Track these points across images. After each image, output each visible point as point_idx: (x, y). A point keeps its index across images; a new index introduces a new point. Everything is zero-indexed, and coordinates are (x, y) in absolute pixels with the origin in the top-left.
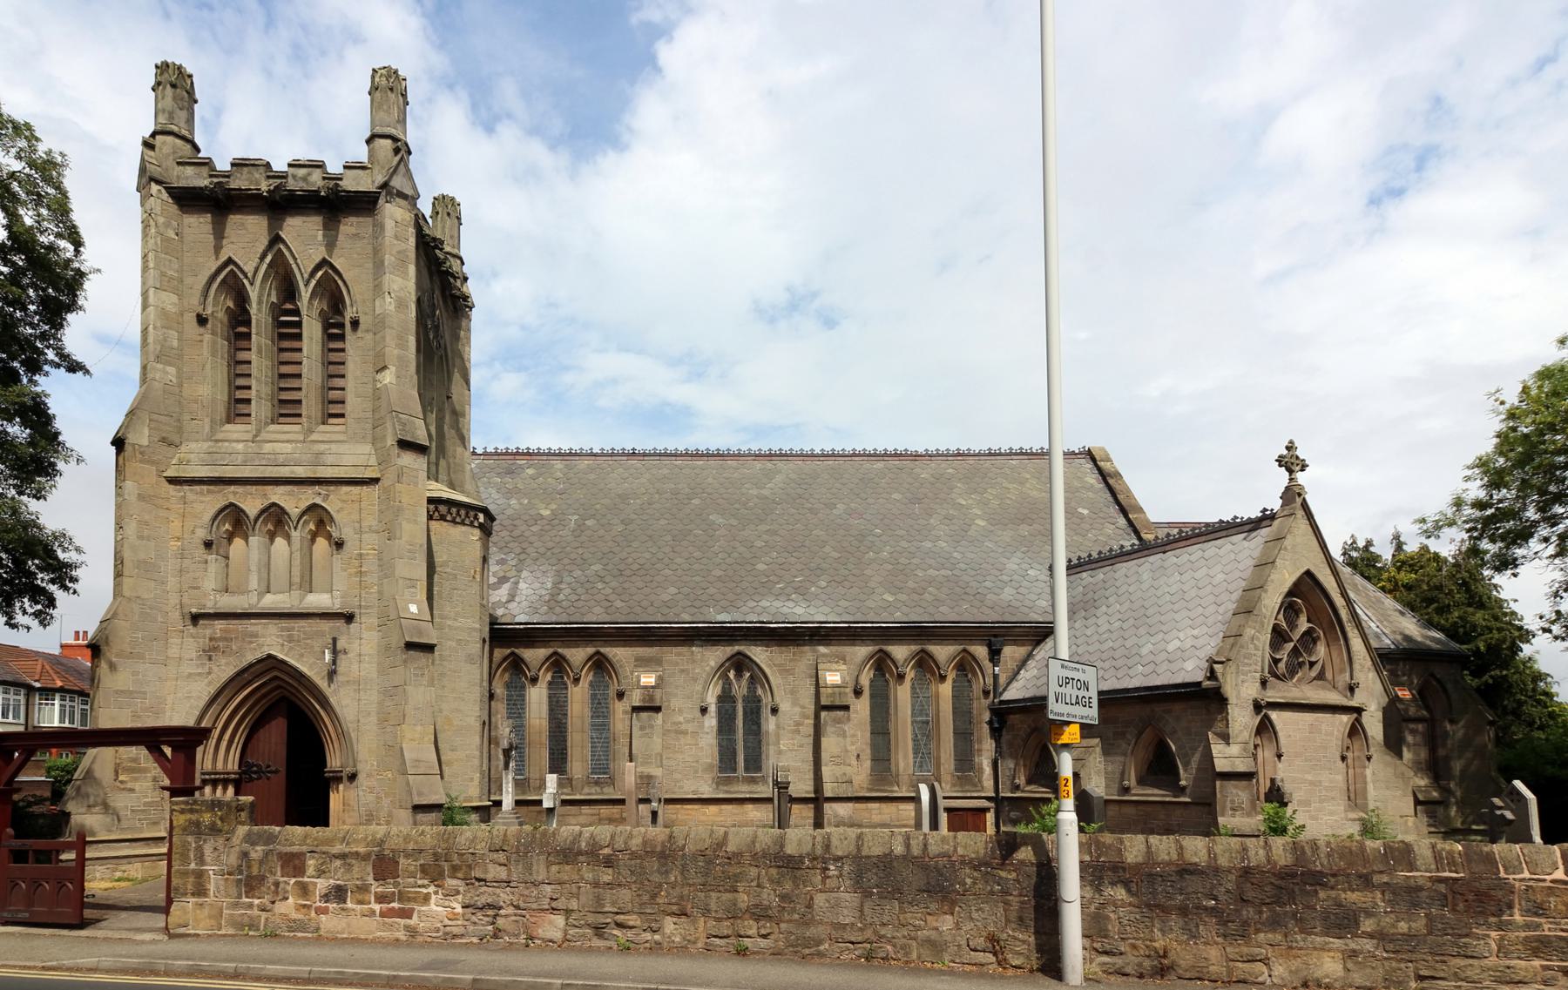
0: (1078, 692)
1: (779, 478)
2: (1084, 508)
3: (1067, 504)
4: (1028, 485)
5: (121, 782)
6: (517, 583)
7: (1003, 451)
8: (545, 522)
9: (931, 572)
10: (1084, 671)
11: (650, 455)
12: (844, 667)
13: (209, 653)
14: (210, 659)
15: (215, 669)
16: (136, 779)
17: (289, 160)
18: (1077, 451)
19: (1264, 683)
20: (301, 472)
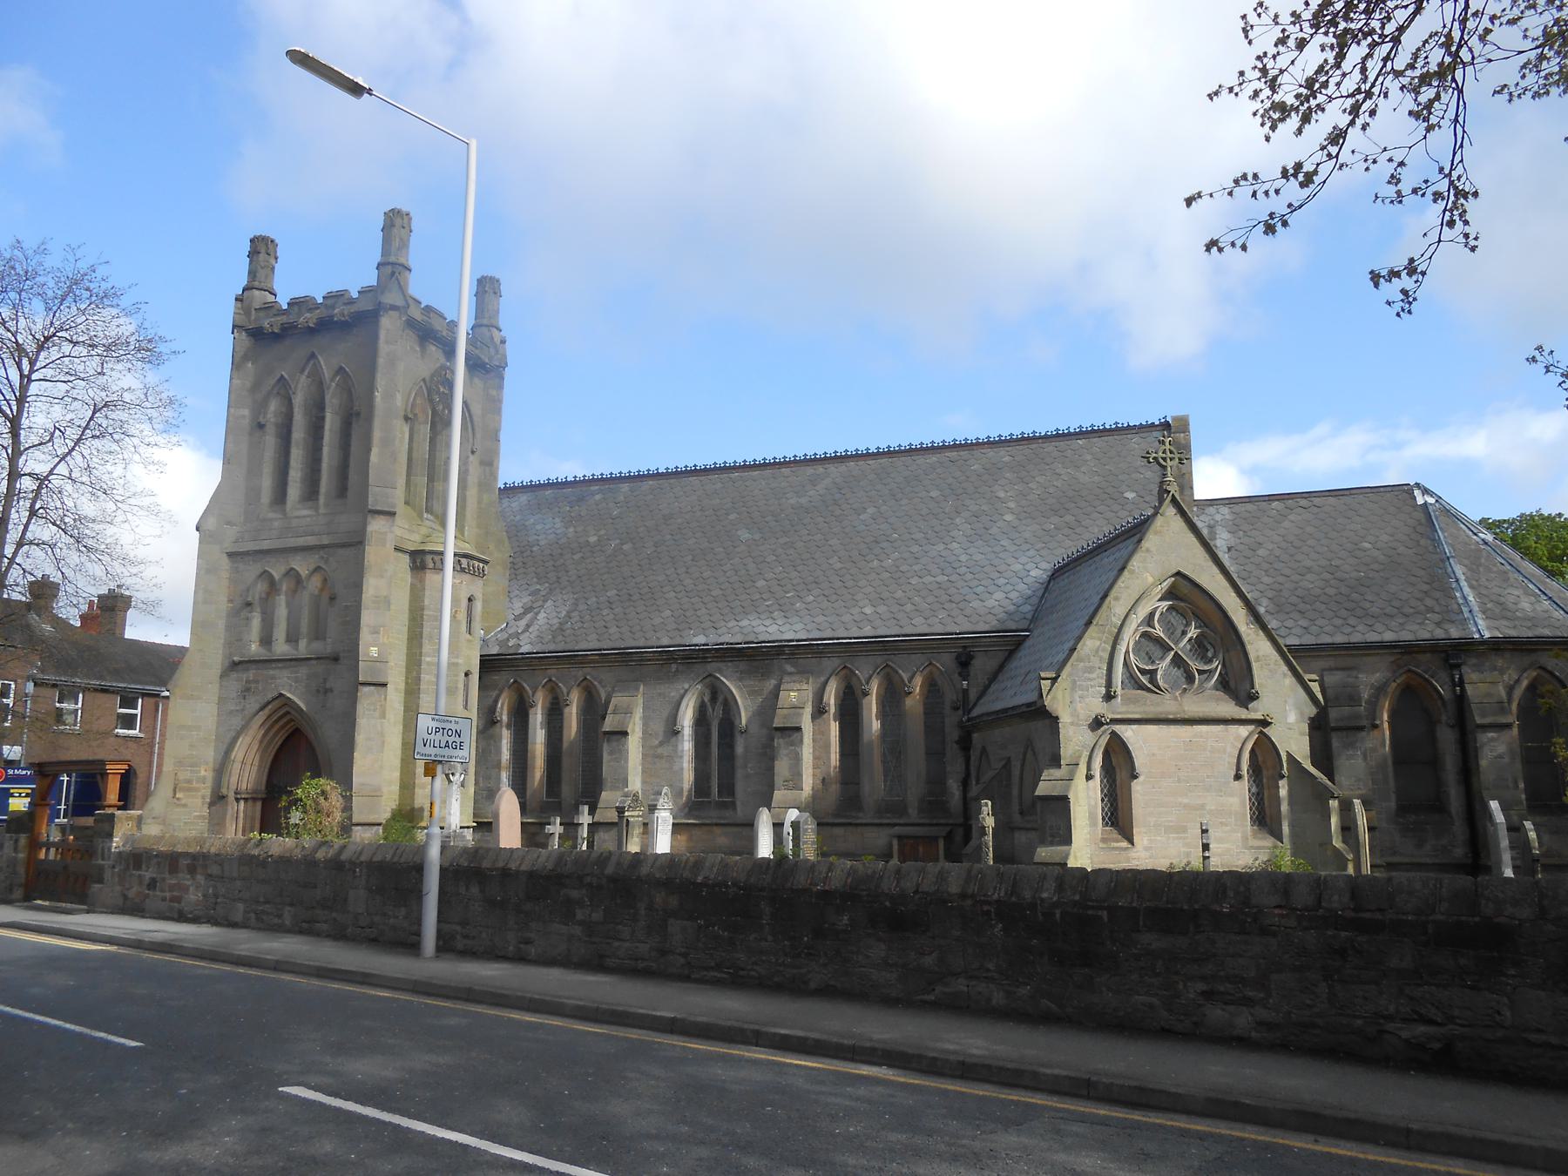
4: (1083, 469)
5: (178, 799)
6: (537, 614)
7: (1072, 431)
12: (805, 686)
13: (246, 691)
14: (244, 699)
15: (248, 706)
19: (1109, 697)
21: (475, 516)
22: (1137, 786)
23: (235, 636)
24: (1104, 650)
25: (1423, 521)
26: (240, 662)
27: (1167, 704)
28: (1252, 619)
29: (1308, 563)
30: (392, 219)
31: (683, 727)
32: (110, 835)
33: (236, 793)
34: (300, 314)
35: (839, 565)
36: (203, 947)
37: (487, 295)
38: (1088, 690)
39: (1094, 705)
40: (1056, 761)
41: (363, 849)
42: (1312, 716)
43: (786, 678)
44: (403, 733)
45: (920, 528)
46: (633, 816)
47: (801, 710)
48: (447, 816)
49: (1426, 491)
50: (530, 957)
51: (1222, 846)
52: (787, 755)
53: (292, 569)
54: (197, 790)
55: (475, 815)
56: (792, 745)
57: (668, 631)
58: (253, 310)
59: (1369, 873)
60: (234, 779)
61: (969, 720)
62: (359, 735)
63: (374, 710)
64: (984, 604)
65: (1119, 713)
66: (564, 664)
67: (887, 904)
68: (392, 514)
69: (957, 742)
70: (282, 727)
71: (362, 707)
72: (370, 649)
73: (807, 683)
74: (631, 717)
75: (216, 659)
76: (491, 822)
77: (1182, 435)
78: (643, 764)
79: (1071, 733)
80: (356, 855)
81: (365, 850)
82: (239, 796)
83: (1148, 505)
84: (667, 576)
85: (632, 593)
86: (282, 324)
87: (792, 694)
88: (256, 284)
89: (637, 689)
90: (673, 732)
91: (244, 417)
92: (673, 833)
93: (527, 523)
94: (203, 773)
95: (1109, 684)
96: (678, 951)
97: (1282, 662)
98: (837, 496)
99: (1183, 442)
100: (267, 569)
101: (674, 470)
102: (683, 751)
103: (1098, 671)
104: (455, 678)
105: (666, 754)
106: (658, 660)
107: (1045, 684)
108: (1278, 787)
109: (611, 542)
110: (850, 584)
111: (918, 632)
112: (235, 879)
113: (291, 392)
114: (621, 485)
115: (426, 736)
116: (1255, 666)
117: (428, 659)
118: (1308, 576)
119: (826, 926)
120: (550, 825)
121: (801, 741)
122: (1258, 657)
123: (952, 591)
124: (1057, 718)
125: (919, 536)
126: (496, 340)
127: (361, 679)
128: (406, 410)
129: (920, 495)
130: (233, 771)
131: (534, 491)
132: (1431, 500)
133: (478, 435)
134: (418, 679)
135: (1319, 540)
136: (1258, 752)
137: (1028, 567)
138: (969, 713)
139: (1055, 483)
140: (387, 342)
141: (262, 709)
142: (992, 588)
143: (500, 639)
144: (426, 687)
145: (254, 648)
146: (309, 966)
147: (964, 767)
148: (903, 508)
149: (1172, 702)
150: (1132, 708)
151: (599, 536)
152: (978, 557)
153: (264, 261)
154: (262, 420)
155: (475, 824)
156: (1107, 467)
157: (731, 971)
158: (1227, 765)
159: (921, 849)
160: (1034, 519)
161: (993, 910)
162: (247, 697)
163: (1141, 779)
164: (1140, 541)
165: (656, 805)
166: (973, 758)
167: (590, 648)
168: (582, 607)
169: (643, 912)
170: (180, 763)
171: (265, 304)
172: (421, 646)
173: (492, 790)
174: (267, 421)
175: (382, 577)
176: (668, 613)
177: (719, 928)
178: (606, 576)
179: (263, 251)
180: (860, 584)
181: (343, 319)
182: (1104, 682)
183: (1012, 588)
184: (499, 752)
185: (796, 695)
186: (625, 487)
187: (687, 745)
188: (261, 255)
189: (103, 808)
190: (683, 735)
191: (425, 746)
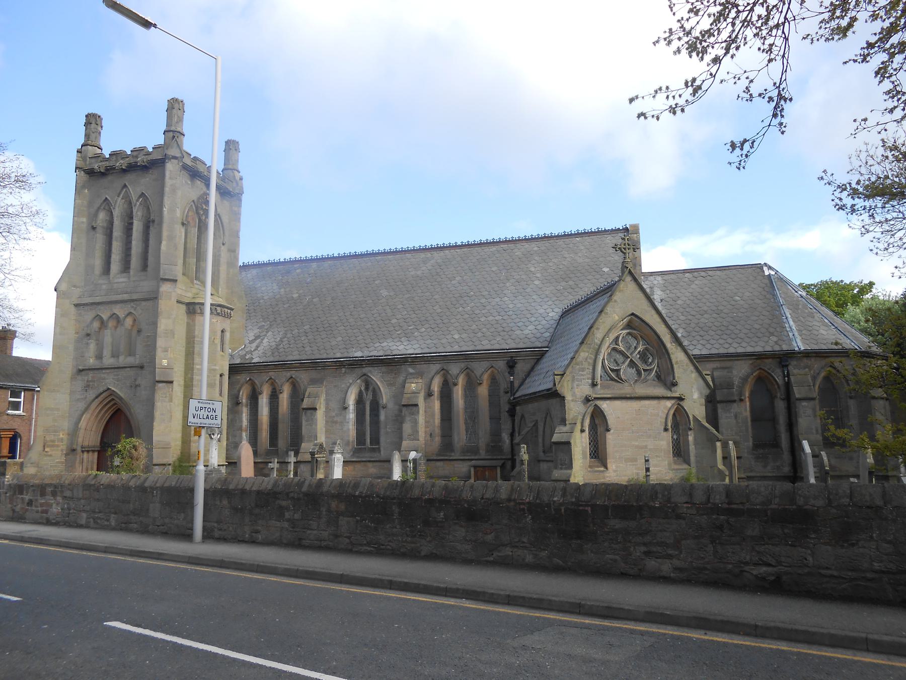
3: (210, 338)
4: (580, 254)
5: (46, 452)
6: (262, 340)
10: (213, 404)
12: (420, 381)
13: (87, 387)
15: (88, 396)
17: (132, 149)
18: (621, 228)
19: (594, 385)
22: (610, 436)
25: (769, 285)
29: (705, 308)
31: (349, 406)
33: (82, 448)
34: (117, 161)
40: (563, 421)
47: (418, 394)
48: (210, 459)
49: (770, 268)
54: (58, 446)
60: (80, 440)
61: (514, 399)
65: (600, 394)
66: (280, 369)
67: (466, 505)
69: (508, 412)
70: (110, 408)
75: (68, 365)
77: (635, 235)
78: (326, 427)
79: (572, 406)
80: (153, 484)
82: (84, 449)
88: (90, 142)
94: (61, 436)
98: (439, 270)
99: (636, 239)
103: (587, 370)
108: (688, 435)
111: (485, 349)
114: (312, 264)
115: (195, 412)
116: (675, 366)
118: (705, 316)
121: (418, 412)
124: (564, 397)
126: (236, 178)
133: (227, 233)
134: (192, 379)
140: (170, 178)
141: (97, 397)
142: (527, 323)
145: (91, 361)
147: (511, 426)
150: (606, 391)
159: (487, 473)
163: (612, 431)
166: (516, 421)
168: (289, 335)
169: (324, 513)
172: (193, 359)
176: (340, 339)
178: (303, 318)
179: (93, 122)
180: (452, 321)
182: (590, 376)
184: (241, 421)
186: (314, 265)
187: (351, 415)
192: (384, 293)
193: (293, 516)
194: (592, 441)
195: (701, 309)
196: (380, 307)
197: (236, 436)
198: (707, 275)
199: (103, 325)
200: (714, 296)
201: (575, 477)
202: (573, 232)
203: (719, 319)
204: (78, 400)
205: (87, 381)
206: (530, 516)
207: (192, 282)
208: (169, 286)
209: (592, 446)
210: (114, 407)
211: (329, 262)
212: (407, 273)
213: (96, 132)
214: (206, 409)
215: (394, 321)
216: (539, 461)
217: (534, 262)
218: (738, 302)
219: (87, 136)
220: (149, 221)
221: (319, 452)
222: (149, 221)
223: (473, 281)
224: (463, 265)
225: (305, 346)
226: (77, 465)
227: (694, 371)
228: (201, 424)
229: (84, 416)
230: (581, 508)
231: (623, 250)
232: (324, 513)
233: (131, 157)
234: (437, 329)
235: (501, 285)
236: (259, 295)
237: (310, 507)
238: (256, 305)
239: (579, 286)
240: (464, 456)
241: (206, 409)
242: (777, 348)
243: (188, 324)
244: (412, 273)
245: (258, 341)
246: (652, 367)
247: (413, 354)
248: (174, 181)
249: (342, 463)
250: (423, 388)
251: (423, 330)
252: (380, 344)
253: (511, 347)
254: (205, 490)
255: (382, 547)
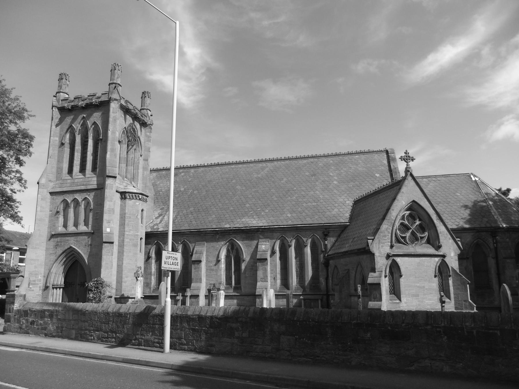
0: (173, 261)
1: (267, 169)
2: (378, 174)
4: (359, 166)
5: (30, 288)
6: (164, 216)
8: (181, 193)
9: (309, 204)
11: (224, 164)
12: (268, 243)
13: (56, 246)
14: (56, 248)
15: (57, 251)
16: (34, 287)
18: (383, 150)
19: (392, 247)
20: (83, 188)
21: (142, 180)
22: (402, 280)
23: (52, 224)
24: (389, 229)
25: (476, 186)
26: (55, 234)
27: (411, 249)
28: (438, 218)
29: (439, 200)
30: (115, 67)
31: (221, 259)
32: (13, 303)
33: (53, 285)
34: (79, 102)
35: (276, 199)
36: (66, 349)
37: (146, 98)
38: (384, 244)
39: (387, 249)
40: (373, 270)
41: (130, 307)
42: (459, 253)
43: (260, 240)
44: (118, 261)
45: (304, 186)
46: (213, 293)
47: (267, 252)
48: (136, 293)
49: (475, 176)
50: (213, 352)
51: (430, 301)
52: (262, 269)
53: (75, 198)
54: (37, 284)
55: (143, 293)
56: (263, 265)
57: (215, 223)
58: (60, 100)
59: (61, 302)
60: (52, 280)
61: (328, 256)
62: (103, 262)
63: (109, 252)
64: (331, 213)
65: (395, 252)
66: (176, 235)
67: (389, 328)
68: (115, 177)
69: (323, 264)
70: (70, 260)
71: (104, 251)
72: (107, 229)
73: (268, 242)
74: (202, 255)
75: (45, 233)
76: (158, 296)
77: (393, 154)
78: (206, 273)
79: (379, 260)
80: (127, 310)
81: (131, 308)
82: (54, 286)
83: (384, 179)
84: (212, 202)
85: (199, 209)
86: (72, 106)
87: (263, 246)
88: (62, 90)
89: (204, 244)
90: (218, 261)
91: (56, 140)
92: (225, 299)
93: (157, 183)
94: (40, 278)
95: (391, 242)
96: (286, 349)
97: (448, 234)
98: (272, 174)
99: (393, 157)
100: (65, 198)
101: (210, 164)
102: (221, 268)
103: (388, 236)
104: (137, 240)
105: (215, 269)
106: (212, 234)
107: (370, 241)
108: (449, 280)
109: (190, 190)
110: (281, 205)
111: (309, 223)
112: (71, 320)
113: (75, 131)
114: (191, 170)
115: (166, 260)
116: (440, 235)
117: (127, 233)
118: (440, 204)
119: (359, 338)
120: (178, 296)
121: (267, 264)
122: (441, 232)
123: (319, 208)
124: (374, 254)
125: (304, 188)
126: (149, 115)
127: (104, 240)
128: (119, 139)
129: (302, 174)
130: (51, 277)
131: (158, 172)
132: (477, 179)
133: (143, 149)
134: (123, 241)
135: (441, 192)
136: (441, 267)
137: (345, 200)
138: (328, 253)
139: (350, 170)
140: (113, 112)
141: (63, 253)
142: (333, 207)
143: (151, 226)
144: (126, 244)
145: (61, 229)
146: (167, 364)
147: (326, 273)
148: (297, 178)
149: (413, 248)
150: (399, 250)
151: (185, 188)
152: (327, 196)
153: (65, 82)
154: (63, 142)
155: (144, 296)
156: (367, 165)
157: (312, 357)
158: (431, 272)
159: (312, 304)
160: (344, 183)
161: (442, 330)
162: (57, 248)
163: (403, 277)
164: (400, 189)
165: (220, 288)
166: (330, 270)
167: (186, 229)
168: (181, 214)
169: (268, 333)
170: (31, 274)
171: (65, 98)
172: (124, 228)
173: (148, 283)
174: (65, 142)
175: (111, 201)
176: (214, 216)
177: (306, 339)
178: (189, 203)
179: (64, 78)
180: (285, 205)
181: (96, 103)
182: (390, 241)
183: (340, 207)
184: (151, 268)
185: (264, 246)
186: (192, 170)
187: (223, 265)
188: (63, 80)
189: (9, 291)
190: (221, 262)
191: (165, 264)
192: (238, 187)
193: (242, 334)
194: (390, 283)
195: (436, 201)
196: (237, 196)
197: (147, 279)
198: (436, 180)
199: (67, 205)
200: (443, 193)
201: (383, 306)
202: (353, 152)
203: (449, 207)
204: (51, 253)
205: (57, 242)
206: (446, 337)
207: (124, 179)
208: (112, 180)
209: (390, 286)
210: (74, 259)
211: (202, 169)
212: (252, 175)
213: (66, 84)
214: (172, 258)
215: (248, 205)
216: (351, 296)
217: (331, 170)
218: (459, 197)
219: (60, 87)
220: (99, 140)
221: (213, 289)
222: (99, 140)
223: (295, 181)
224: (287, 171)
225: (192, 221)
226: (50, 297)
227: (451, 238)
228: (169, 268)
229: (55, 264)
230: (491, 331)
231: (406, 160)
232: (268, 333)
233: (88, 100)
234: (276, 211)
235: (313, 183)
236: (159, 189)
237: (256, 328)
238: (157, 195)
239: (362, 185)
240: (296, 292)
241: (172, 258)
242: (488, 225)
243: (121, 205)
244: (255, 176)
245: (161, 217)
246: (426, 234)
247: (263, 226)
248: (115, 115)
249: (224, 297)
250: (270, 248)
251: (267, 211)
252: (240, 220)
253: (325, 223)
254: (172, 316)
255: (317, 358)
